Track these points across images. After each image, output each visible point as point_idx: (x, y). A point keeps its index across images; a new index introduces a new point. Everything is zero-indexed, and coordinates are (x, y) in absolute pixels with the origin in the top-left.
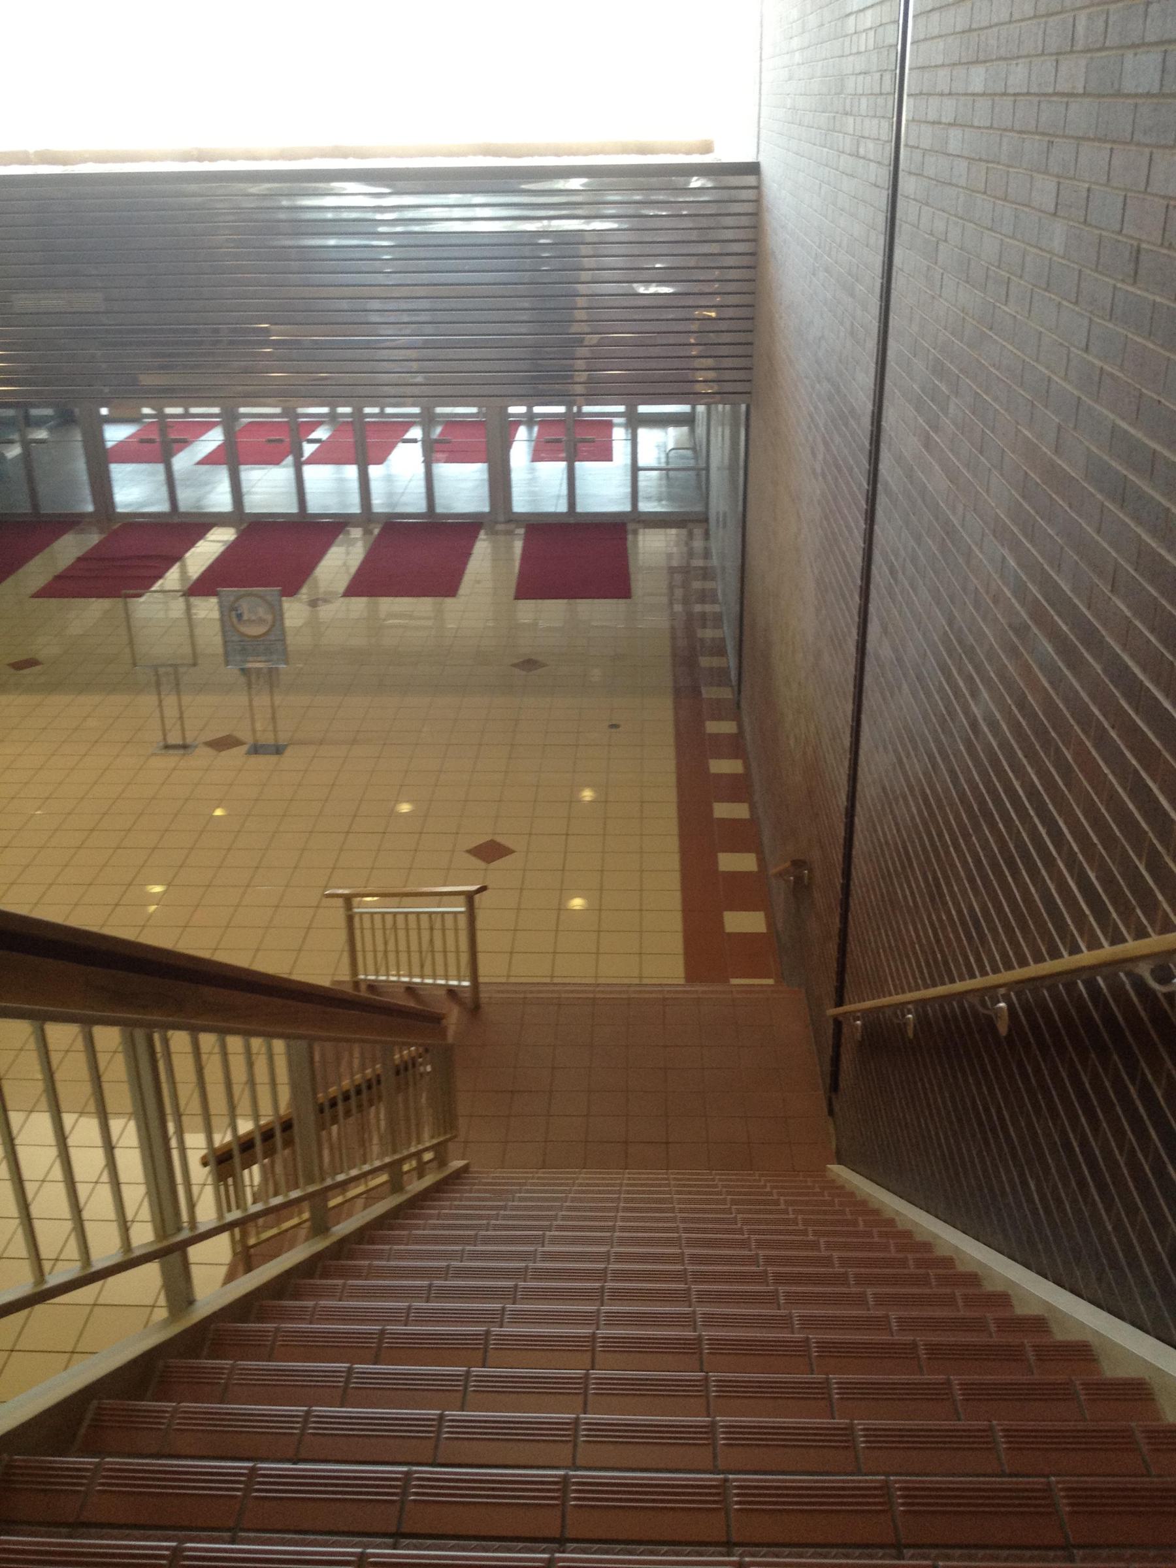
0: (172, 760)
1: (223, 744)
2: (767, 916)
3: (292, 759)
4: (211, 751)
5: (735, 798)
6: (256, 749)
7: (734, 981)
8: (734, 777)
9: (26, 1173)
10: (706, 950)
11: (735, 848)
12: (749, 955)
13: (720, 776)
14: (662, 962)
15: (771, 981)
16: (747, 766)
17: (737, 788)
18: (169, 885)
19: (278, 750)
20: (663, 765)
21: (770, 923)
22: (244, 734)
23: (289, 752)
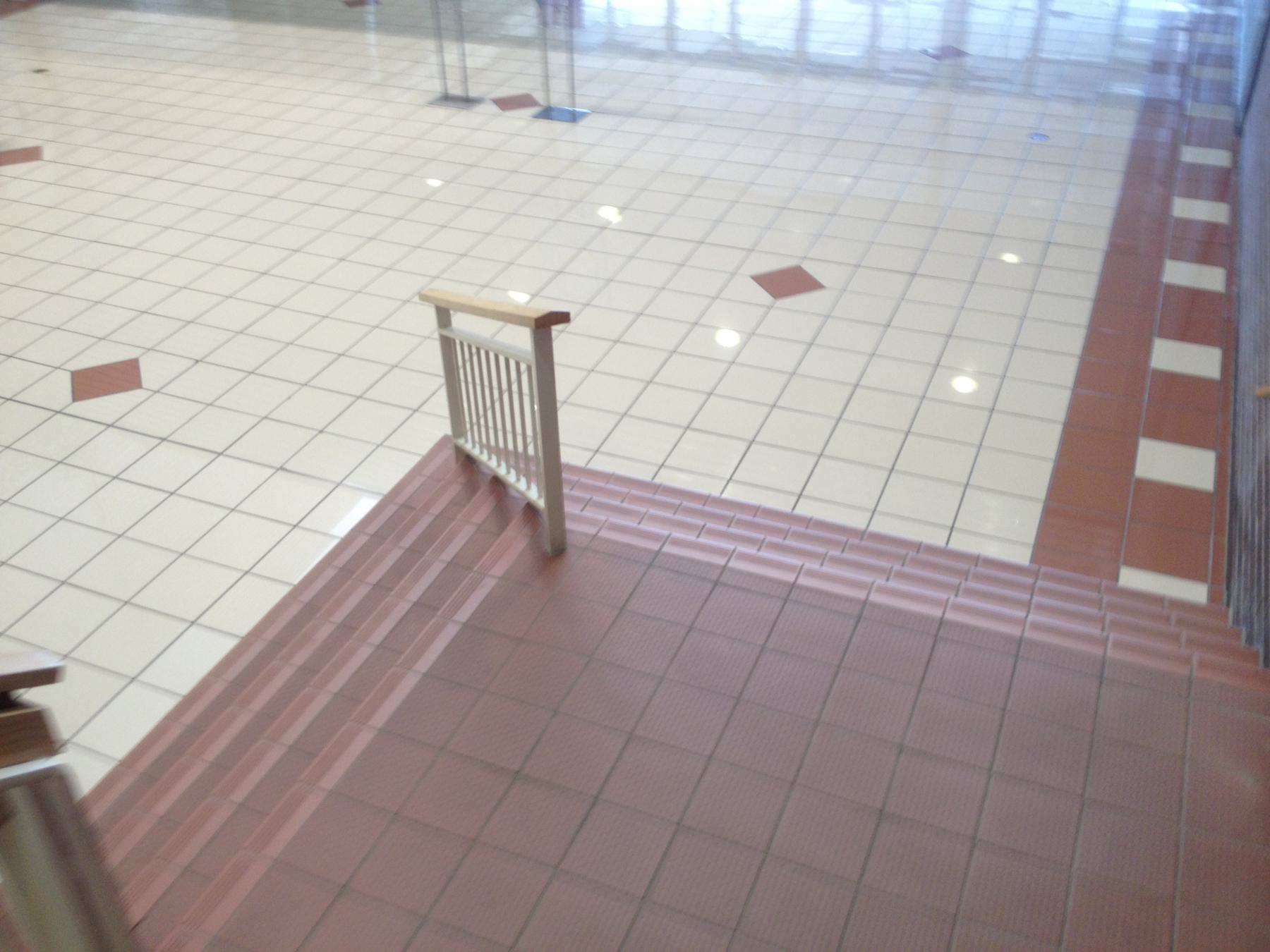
0: (442, 113)
1: (506, 104)
2: (1220, 462)
3: (582, 132)
4: (495, 109)
5: (1204, 257)
6: (547, 113)
7: (1132, 578)
8: (1212, 228)
9: (576, 77)
10: (1090, 504)
11: (1187, 332)
12: (1171, 526)
13: (1186, 223)
14: (1004, 527)
15: (1196, 592)
16: (1235, 214)
17: (1213, 245)
18: (448, 182)
19: (574, 117)
20: (1094, 205)
21: (1226, 473)
22: (539, 96)
23: (583, 123)
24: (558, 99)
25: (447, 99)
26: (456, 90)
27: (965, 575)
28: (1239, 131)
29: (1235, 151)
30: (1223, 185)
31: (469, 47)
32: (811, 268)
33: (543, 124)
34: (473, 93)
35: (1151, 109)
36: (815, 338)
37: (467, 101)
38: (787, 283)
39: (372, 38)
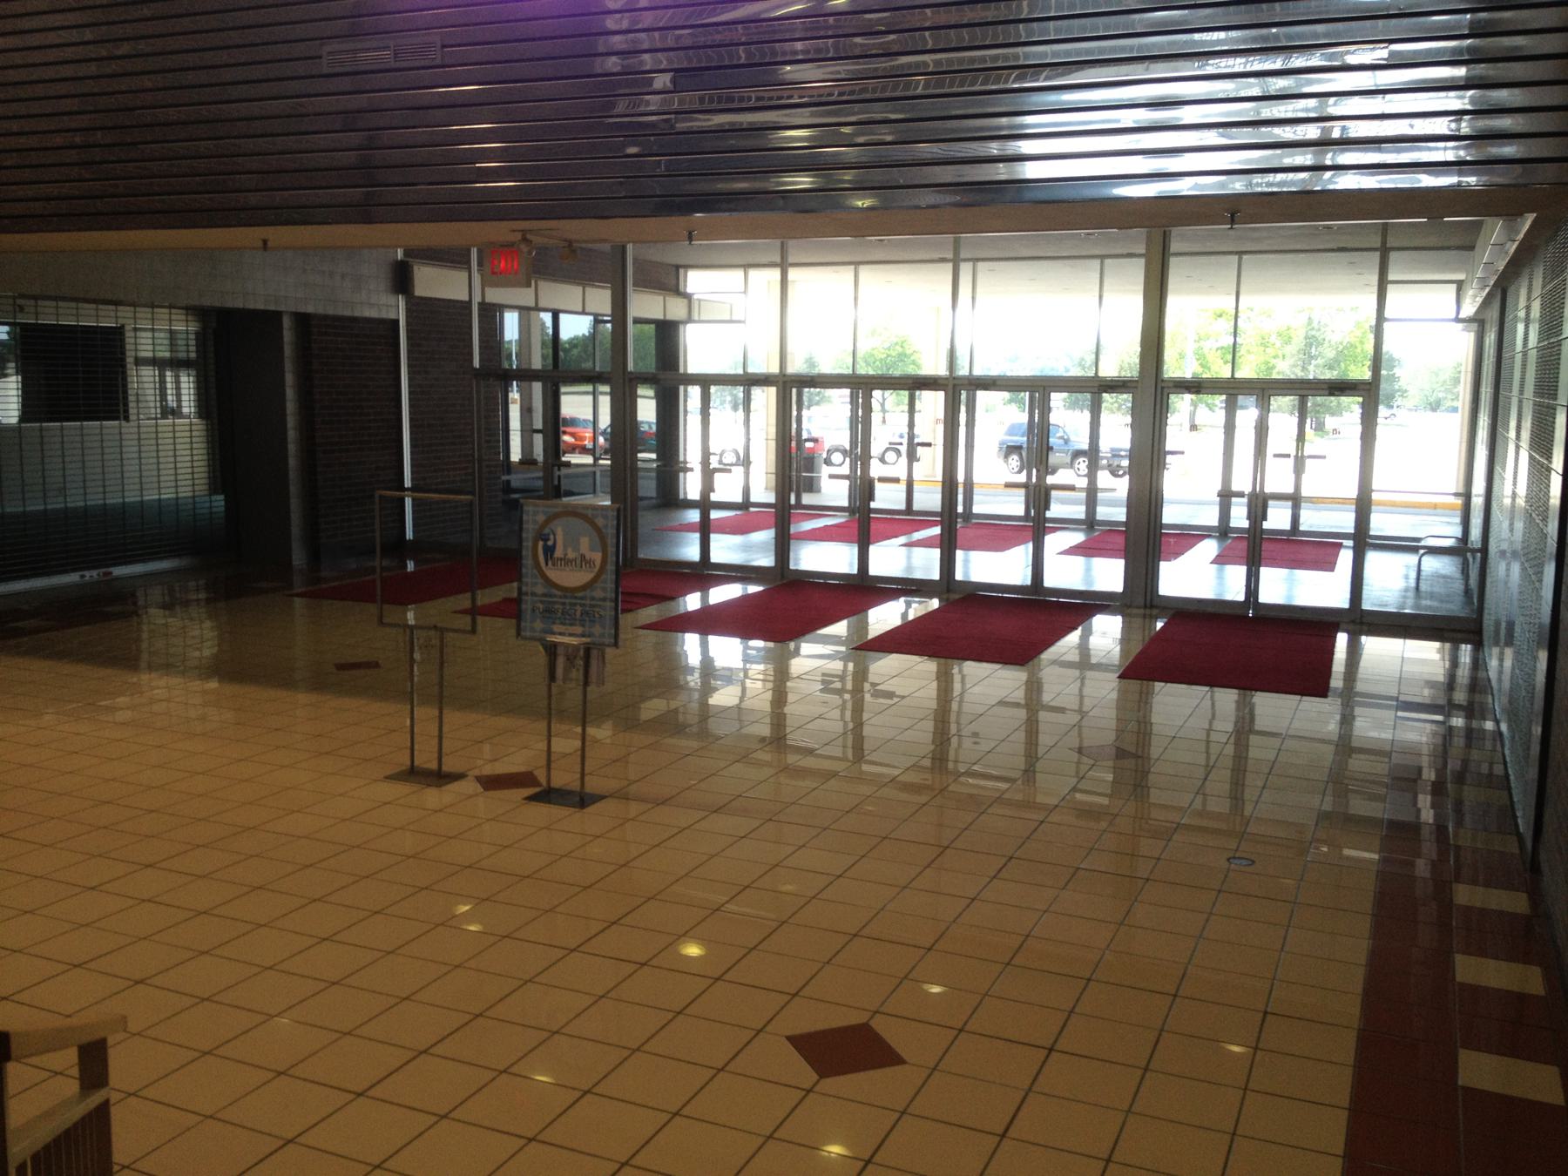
0: (401, 789)
1: (493, 783)
6: (548, 795)
19: (582, 800)
22: (541, 776)
24: (563, 778)
25: (413, 774)
26: (427, 760)
27: (1324, 143)
28: (1535, 867)
29: (1536, 895)
30: (1524, 939)
31: (453, 718)
32: (886, 1029)
33: (542, 811)
34: (449, 765)
35: (1394, 903)
36: (1007, 1130)
37: (440, 777)
38: (844, 1051)
39: (303, 698)
